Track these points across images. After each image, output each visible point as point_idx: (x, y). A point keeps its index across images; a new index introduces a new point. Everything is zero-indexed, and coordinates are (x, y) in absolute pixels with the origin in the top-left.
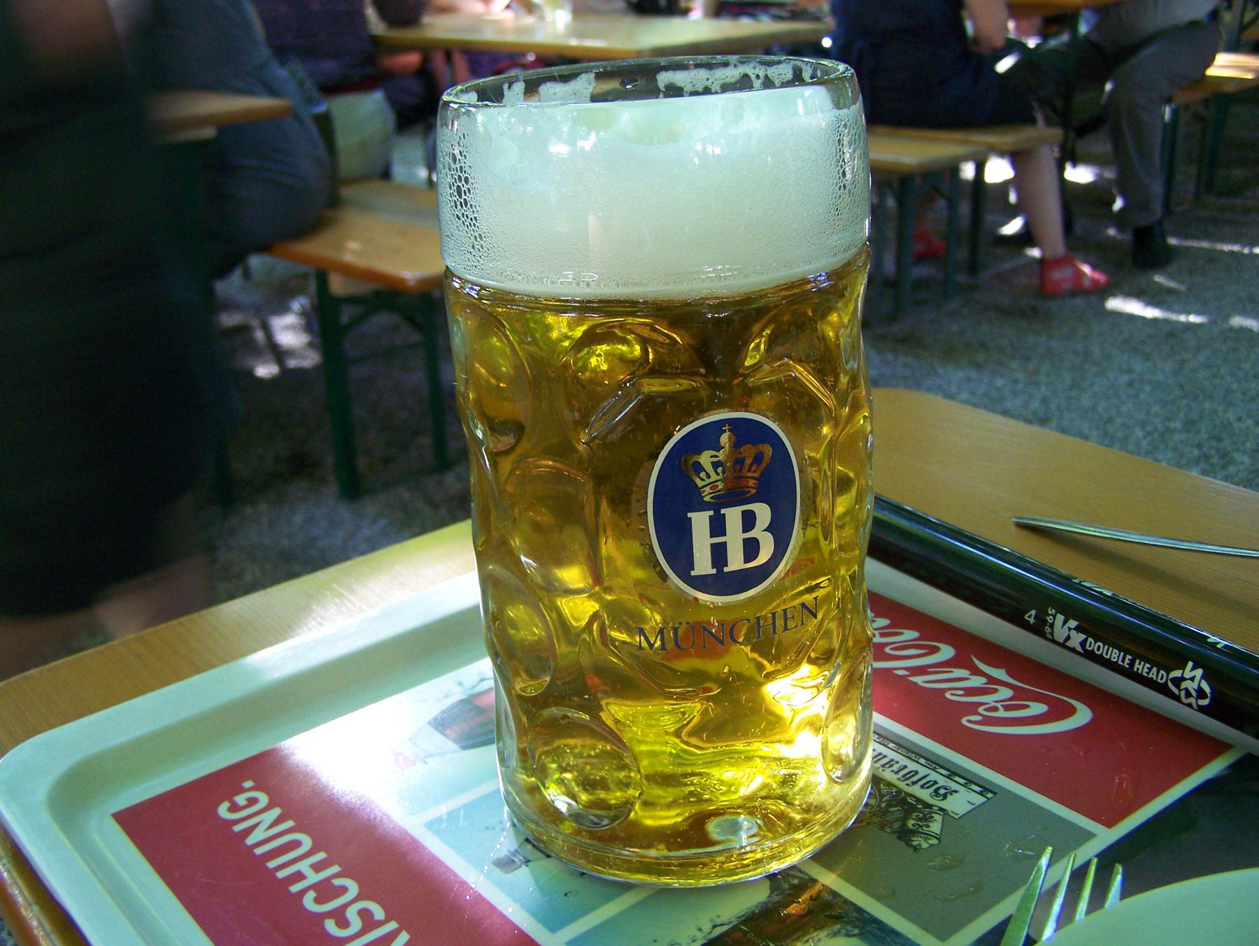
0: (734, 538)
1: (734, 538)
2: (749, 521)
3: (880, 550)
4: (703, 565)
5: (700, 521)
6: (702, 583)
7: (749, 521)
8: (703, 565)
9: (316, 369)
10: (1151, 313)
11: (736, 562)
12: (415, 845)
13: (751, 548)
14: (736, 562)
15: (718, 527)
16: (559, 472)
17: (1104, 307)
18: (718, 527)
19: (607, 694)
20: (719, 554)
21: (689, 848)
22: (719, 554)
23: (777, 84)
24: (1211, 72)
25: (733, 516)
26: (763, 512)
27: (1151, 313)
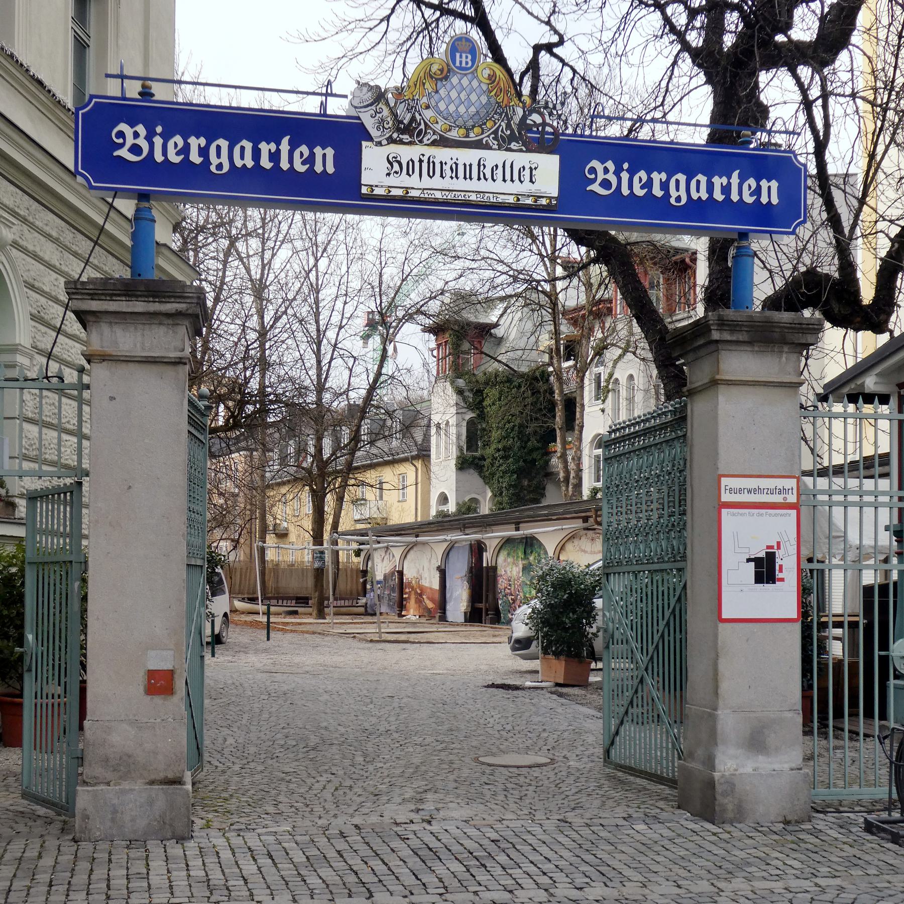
0: (464, 60)
1: (464, 60)
2: (467, 57)
4: (458, 64)
5: (458, 55)
6: (457, 67)
7: (467, 57)
8: (458, 64)
11: (464, 65)
13: (467, 63)
14: (464, 65)
15: (461, 57)
16: (677, 375)
17: (868, 306)
18: (461, 57)
19: (711, 240)
20: (461, 62)
22: (461, 62)
23: (83, 637)
24: (288, 137)
25: (464, 55)
26: (470, 57)
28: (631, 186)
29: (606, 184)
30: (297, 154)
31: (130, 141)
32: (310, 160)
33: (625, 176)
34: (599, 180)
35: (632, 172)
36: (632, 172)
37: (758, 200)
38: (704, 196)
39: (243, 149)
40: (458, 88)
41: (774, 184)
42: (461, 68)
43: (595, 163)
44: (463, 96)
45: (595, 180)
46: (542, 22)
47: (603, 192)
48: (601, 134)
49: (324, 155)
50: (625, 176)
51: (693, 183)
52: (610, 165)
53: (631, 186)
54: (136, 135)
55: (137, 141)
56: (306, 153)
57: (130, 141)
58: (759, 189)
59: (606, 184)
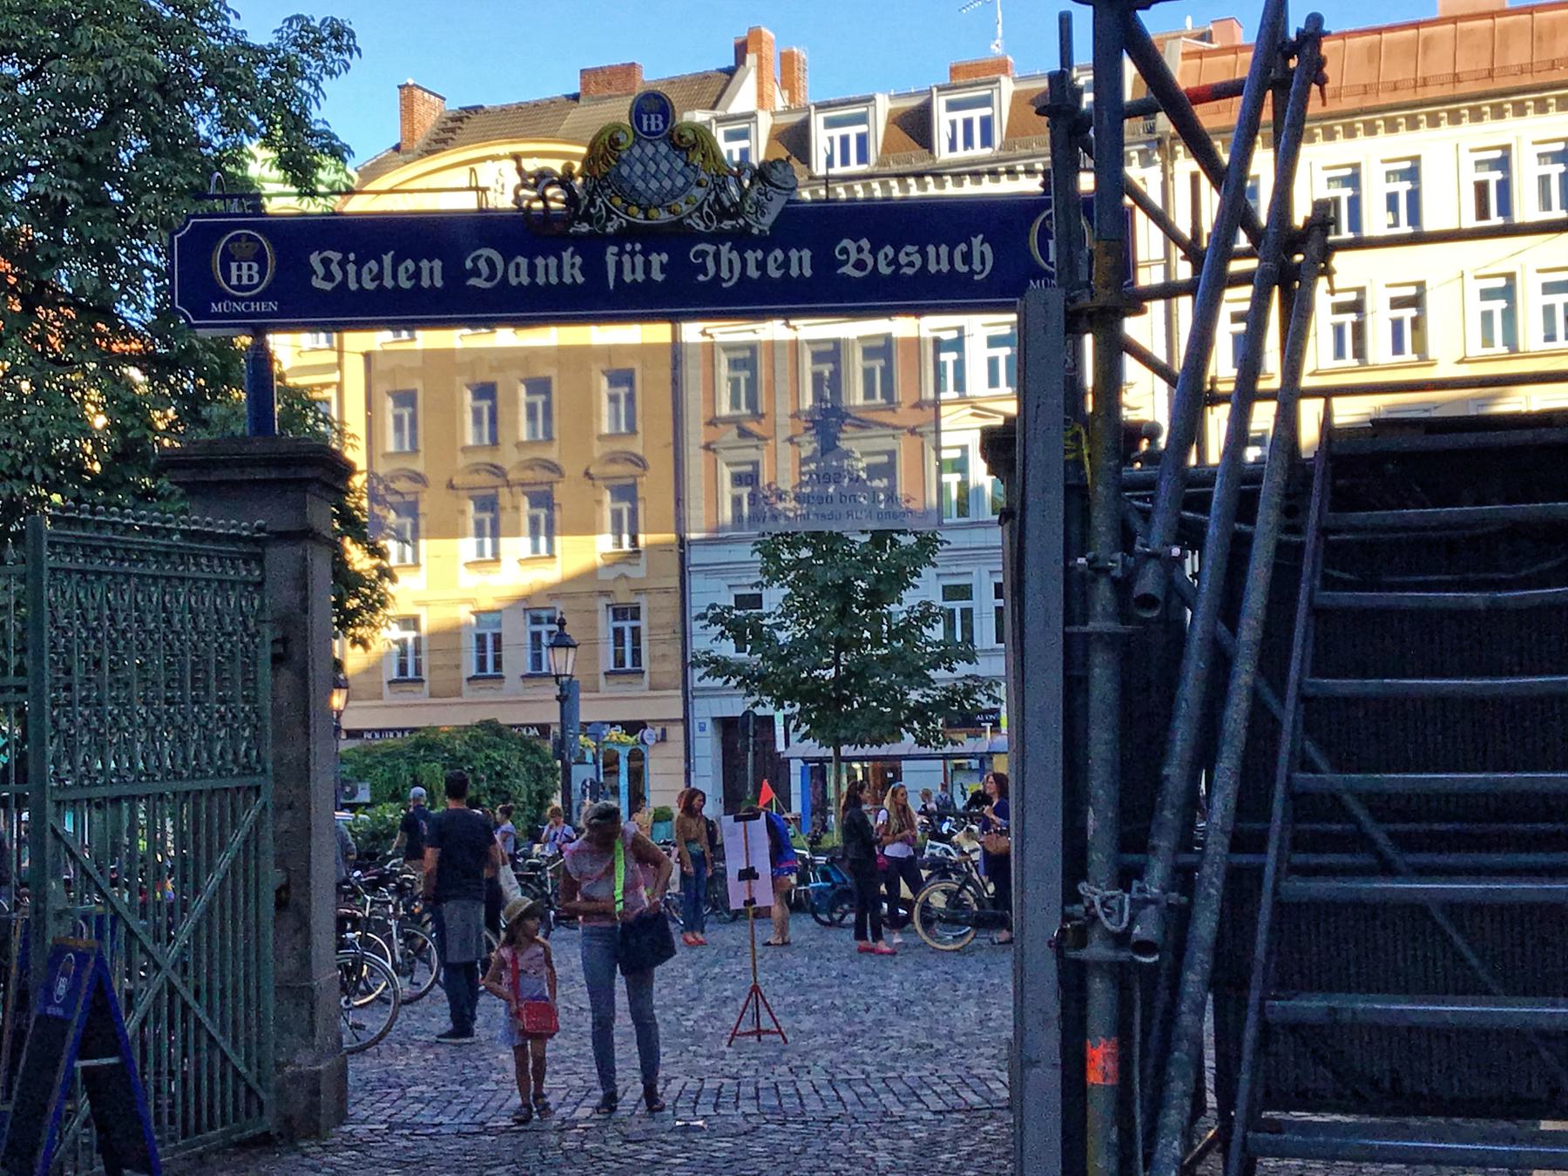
0: (245, 272)
1: (245, 272)
2: (250, 268)
3: (494, 635)
4: (645, 128)
7: (250, 268)
9: (1290, 227)
10: (1089, 381)
11: (245, 281)
12: (305, 214)
13: (250, 278)
14: (245, 281)
15: (239, 268)
17: (1119, 327)
18: (239, 268)
20: (239, 277)
21: (1296, 601)
22: (239, 277)
25: (245, 265)
26: (255, 266)
27: (1089, 381)
28: (359, 280)
29: (860, 265)
30: (401, 269)
31: (854, 256)
32: (416, 276)
33: (351, 268)
34: (852, 261)
35: (360, 264)
36: (360, 264)
37: (787, 273)
38: (640, 277)
39: (518, 266)
40: (658, 157)
41: (437, 264)
42: (649, 133)
43: (846, 243)
44: (652, 168)
45: (847, 261)
46: (729, 82)
47: (858, 274)
48: (357, 205)
49: (800, 259)
50: (351, 268)
51: (512, 268)
52: (865, 243)
53: (359, 280)
54: (860, 250)
55: (862, 256)
56: (781, 257)
57: (854, 256)
58: (418, 271)
59: (860, 265)
